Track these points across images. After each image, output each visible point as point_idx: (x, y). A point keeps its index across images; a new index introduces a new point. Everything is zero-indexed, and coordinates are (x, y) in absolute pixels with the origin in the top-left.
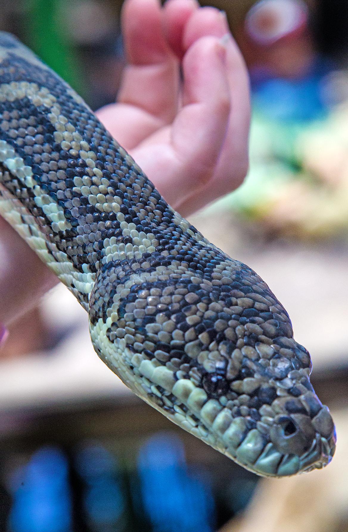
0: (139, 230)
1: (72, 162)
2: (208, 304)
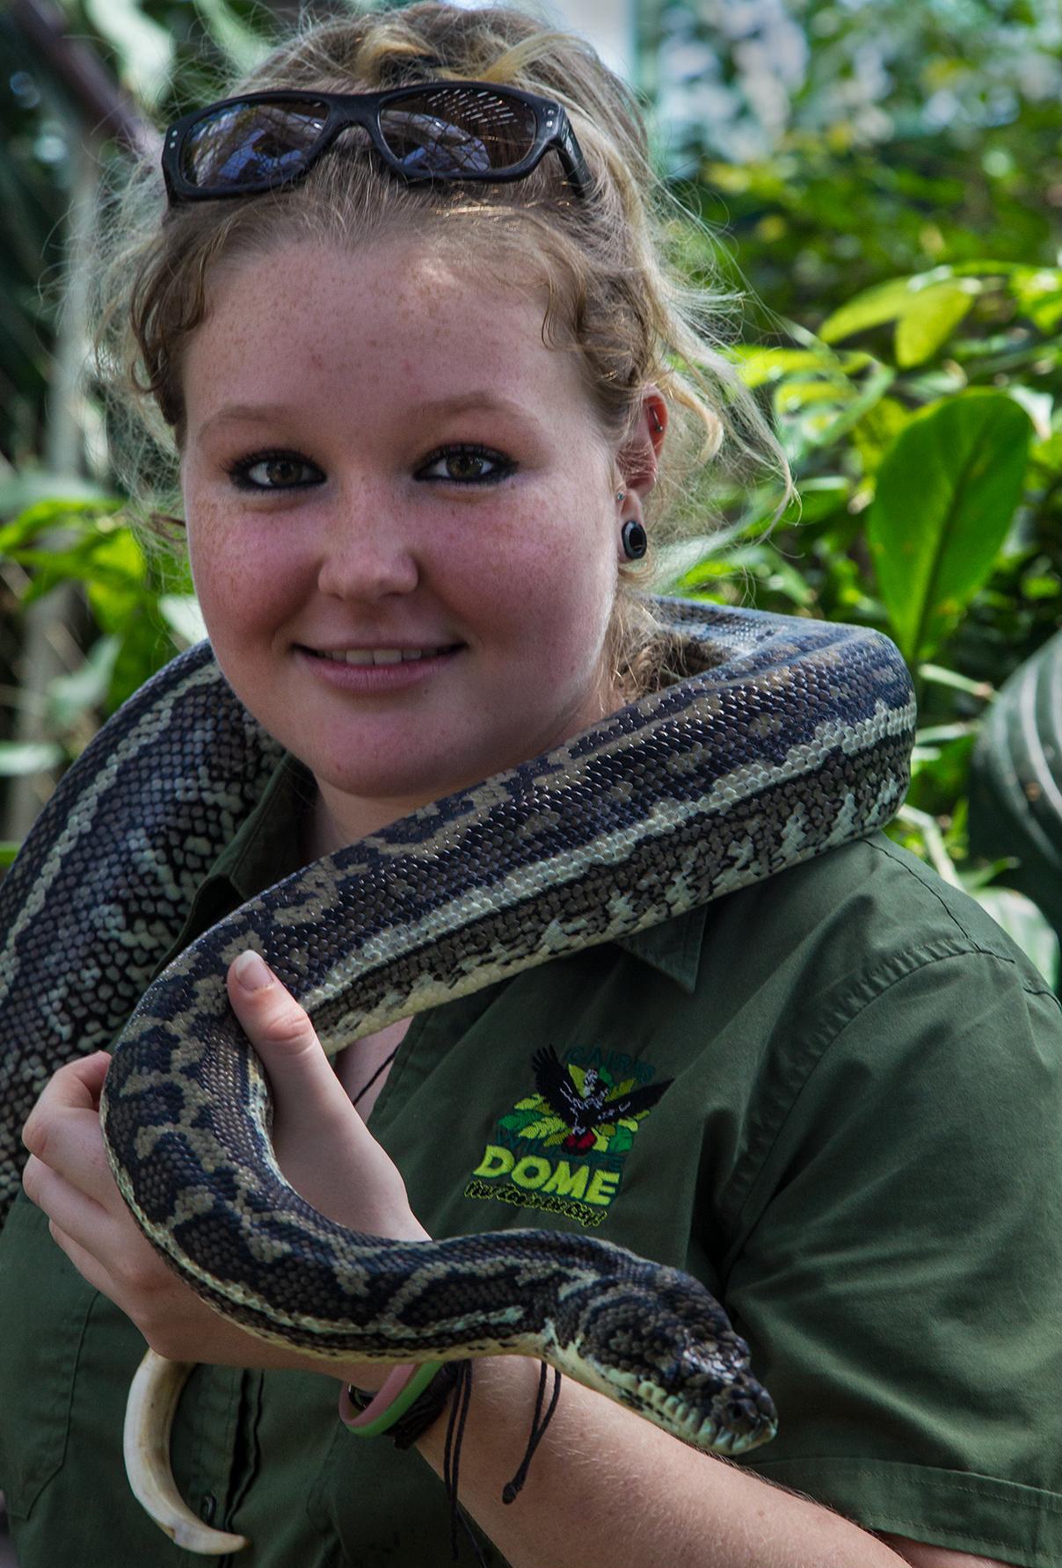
1: (525, 1105)
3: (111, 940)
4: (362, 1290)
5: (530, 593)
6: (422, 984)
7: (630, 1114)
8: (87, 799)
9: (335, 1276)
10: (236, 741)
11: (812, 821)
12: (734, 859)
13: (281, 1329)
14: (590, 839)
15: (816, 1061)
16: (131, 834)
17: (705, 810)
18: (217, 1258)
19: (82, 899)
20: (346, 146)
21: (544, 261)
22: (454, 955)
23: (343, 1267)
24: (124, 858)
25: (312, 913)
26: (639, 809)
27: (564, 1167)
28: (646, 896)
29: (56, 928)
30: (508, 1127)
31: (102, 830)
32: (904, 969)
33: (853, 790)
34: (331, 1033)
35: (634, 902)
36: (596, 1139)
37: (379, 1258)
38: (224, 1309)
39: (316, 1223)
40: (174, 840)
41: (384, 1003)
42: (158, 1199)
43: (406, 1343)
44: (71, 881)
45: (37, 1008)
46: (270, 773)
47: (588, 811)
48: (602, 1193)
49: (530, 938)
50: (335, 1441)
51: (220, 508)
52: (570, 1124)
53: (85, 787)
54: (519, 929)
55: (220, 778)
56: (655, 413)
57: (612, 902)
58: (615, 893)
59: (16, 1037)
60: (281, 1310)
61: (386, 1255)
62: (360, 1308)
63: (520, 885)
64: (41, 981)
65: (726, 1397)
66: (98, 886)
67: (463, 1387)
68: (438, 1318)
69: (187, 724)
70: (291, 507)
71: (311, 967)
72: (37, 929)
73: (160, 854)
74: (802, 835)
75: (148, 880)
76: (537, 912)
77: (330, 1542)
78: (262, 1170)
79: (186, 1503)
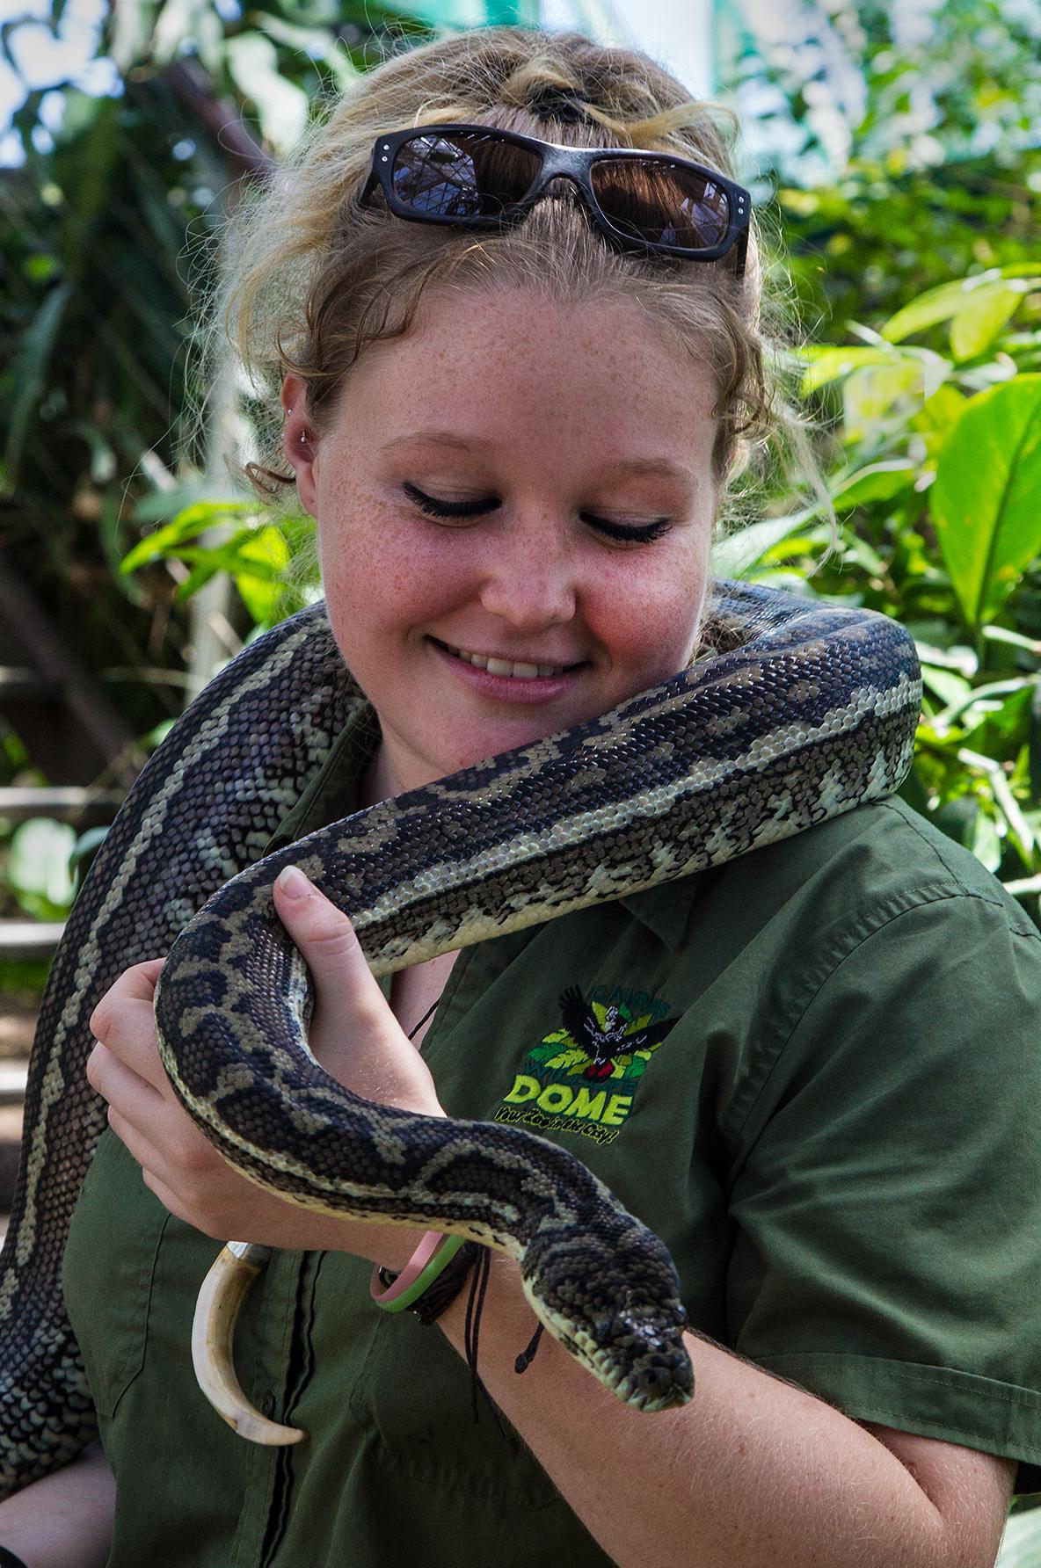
0: (567, 1207)
2: (606, 1273)
4: (400, 1160)
7: (646, 1046)
9: (375, 1146)
13: (320, 1194)
14: (633, 793)
15: (814, 994)
16: (199, 833)
17: (743, 768)
18: (260, 1129)
22: (502, 892)
27: (584, 1093)
29: (133, 922)
30: (537, 1059)
31: (172, 832)
32: (897, 911)
33: (883, 748)
35: (675, 852)
36: (614, 1069)
38: (264, 1177)
40: (237, 837)
41: (431, 934)
42: (200, 1074)
48: (616, 1115)
49: (578, 880)
50: (375, 1341)
52: (592, 1056)
53: (156, 791)
55: (274, 776)
58: (658, 844)
62: (397, 1175)
63: (567, 832)
65: (646, 1362)
66: (170, 883)
67: (483, 1265)
72: (115, 924)
73: (225, 850)
75: (214, 875)
76: (581, 857)
77: (372, 1434)
79: (250, 1401)
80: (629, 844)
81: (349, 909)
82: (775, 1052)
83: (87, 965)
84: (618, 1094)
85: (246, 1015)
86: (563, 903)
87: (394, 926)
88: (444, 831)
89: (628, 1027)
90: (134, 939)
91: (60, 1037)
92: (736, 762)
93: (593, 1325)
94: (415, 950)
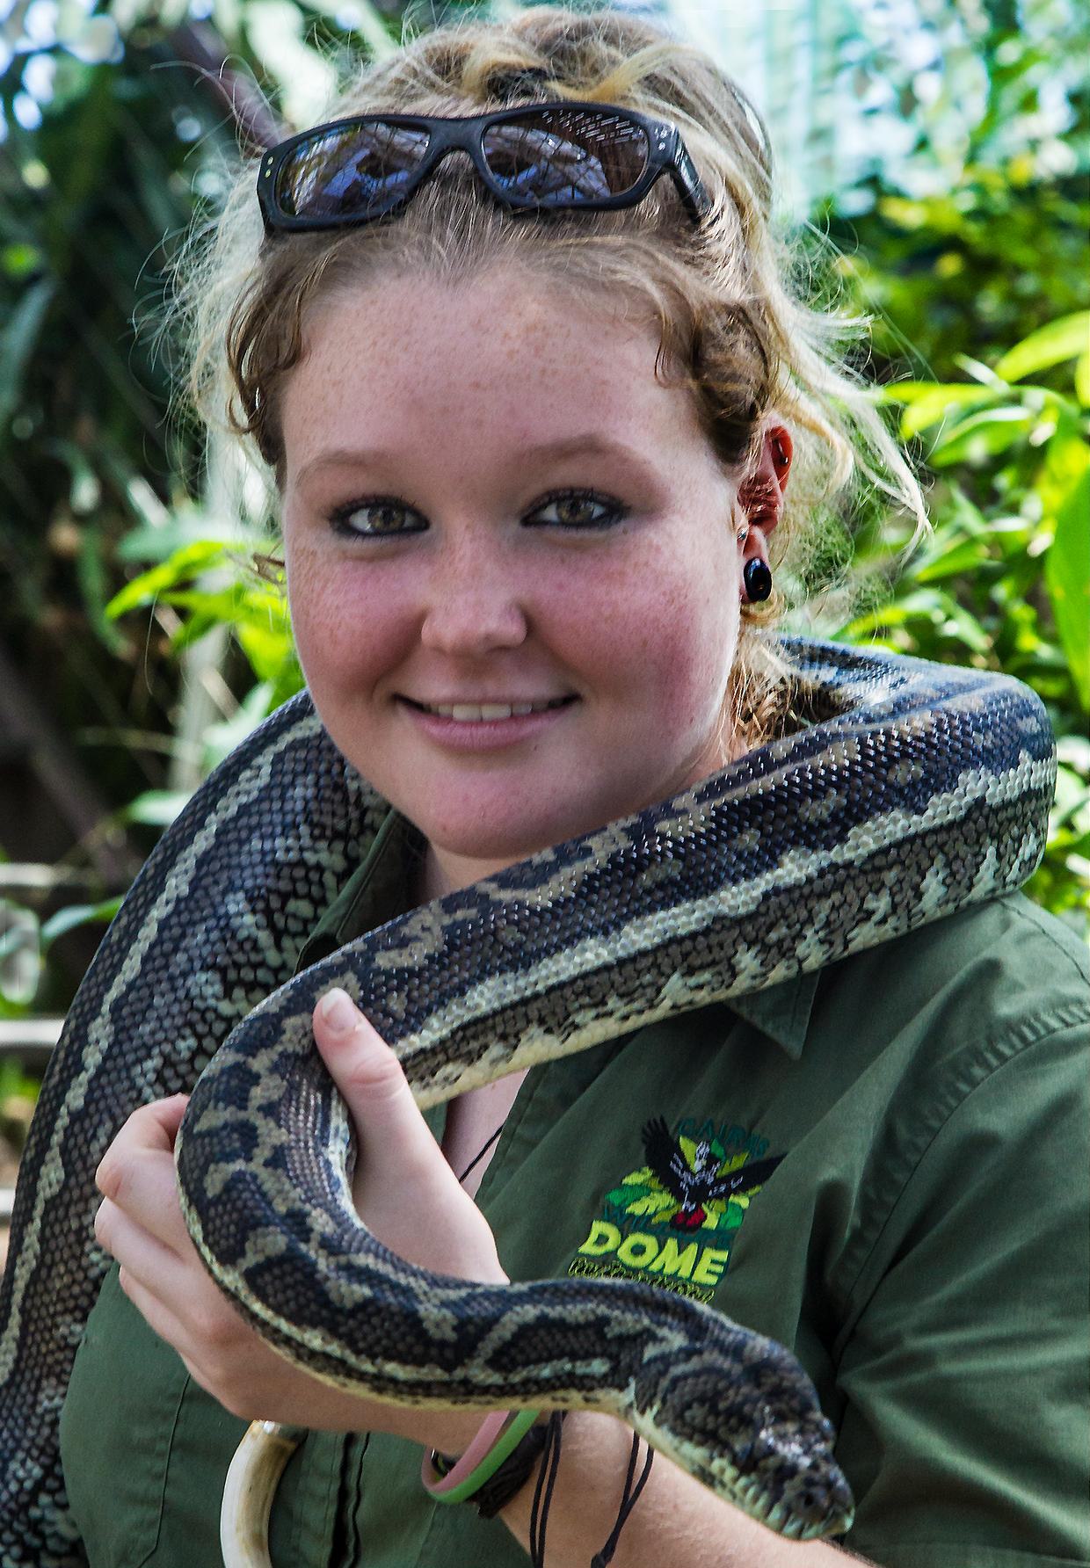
3: (207, 1009)
4: (451, 1335)
5: (645, 643)
6: (531, 1038)
7: (742, 1189)
8: (185, 861)
9: (419, 1321)
10: (338, 797)
11: (953, 874)
12: (870, 913)
13: (362, 1377)
15: (935, 1133)
16: (230, 897)
17: (840, 861)
19: (179, 965)
20: (449, 173)
21: (656, 294)
23: (429, 1311)
24: (222, 923)
25: (414, 957)
26: (768, 858)
27: (672, 1244)
28: (774, 951)
29: (152, 996)
31: (199, 894)
33: (995, 843)
34: (428, 1085)
35: (761, 957)
37: (467, 1301)
38: (299, 1357)
39: (395, 1267)
41: (488, 1056)
42: (227, 1239)
43: (493, 1390)
44: (168, 946)
45: (131, 1080)
46: (375, 832)
47: (713, 860)
49: (650, 992)
51: (319, 555)
52: (680, 1199)
53: (183, 848)
54: (637, 983)
55: (322, 837)
56: (780, 447)
57: (738, 955)
58: (742, 947)
59: (109, 1109)
60: (363, 1357)
61: (471, 1298)
62: (449, 1354)
63: (640, 935)
64: (136, 1050)
68: (526, 1364)
69: (288, 779)
70: (395, 555)
71: (408, 1013)
72: (132, 997)
73: (260, 918)
74: (942, 890)
75: (248, 946)
76: (656, 965)
78: (337, 1212)
80: (710, 948)
81: (390, 1041)
82: (891, 1199)
83: (97, 1042)
84: (711, 1247)
85: (280, 1171)
86: (633, 1018)
87: (445, 1051)
88: (499, 937)
89: (722, 1167)
90: (152, 1014)
91: (62, 1122)
92: (832, 853)
93: (731, 1449)
94: (467, 1076)
